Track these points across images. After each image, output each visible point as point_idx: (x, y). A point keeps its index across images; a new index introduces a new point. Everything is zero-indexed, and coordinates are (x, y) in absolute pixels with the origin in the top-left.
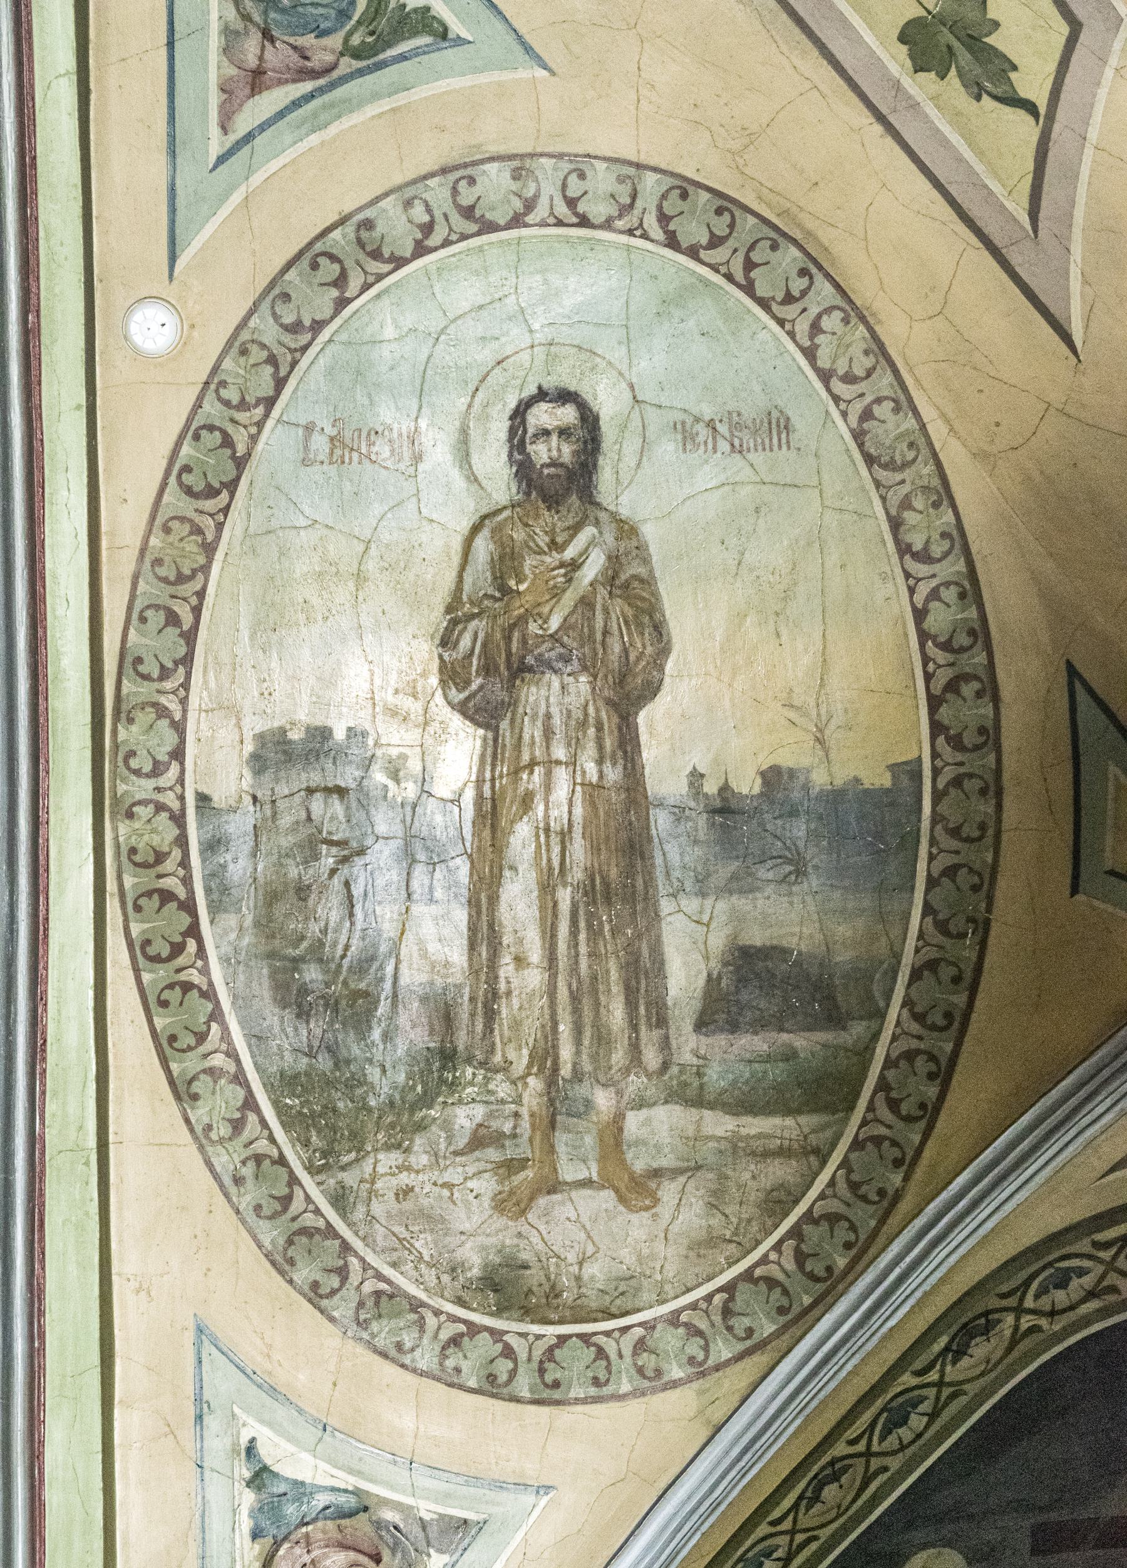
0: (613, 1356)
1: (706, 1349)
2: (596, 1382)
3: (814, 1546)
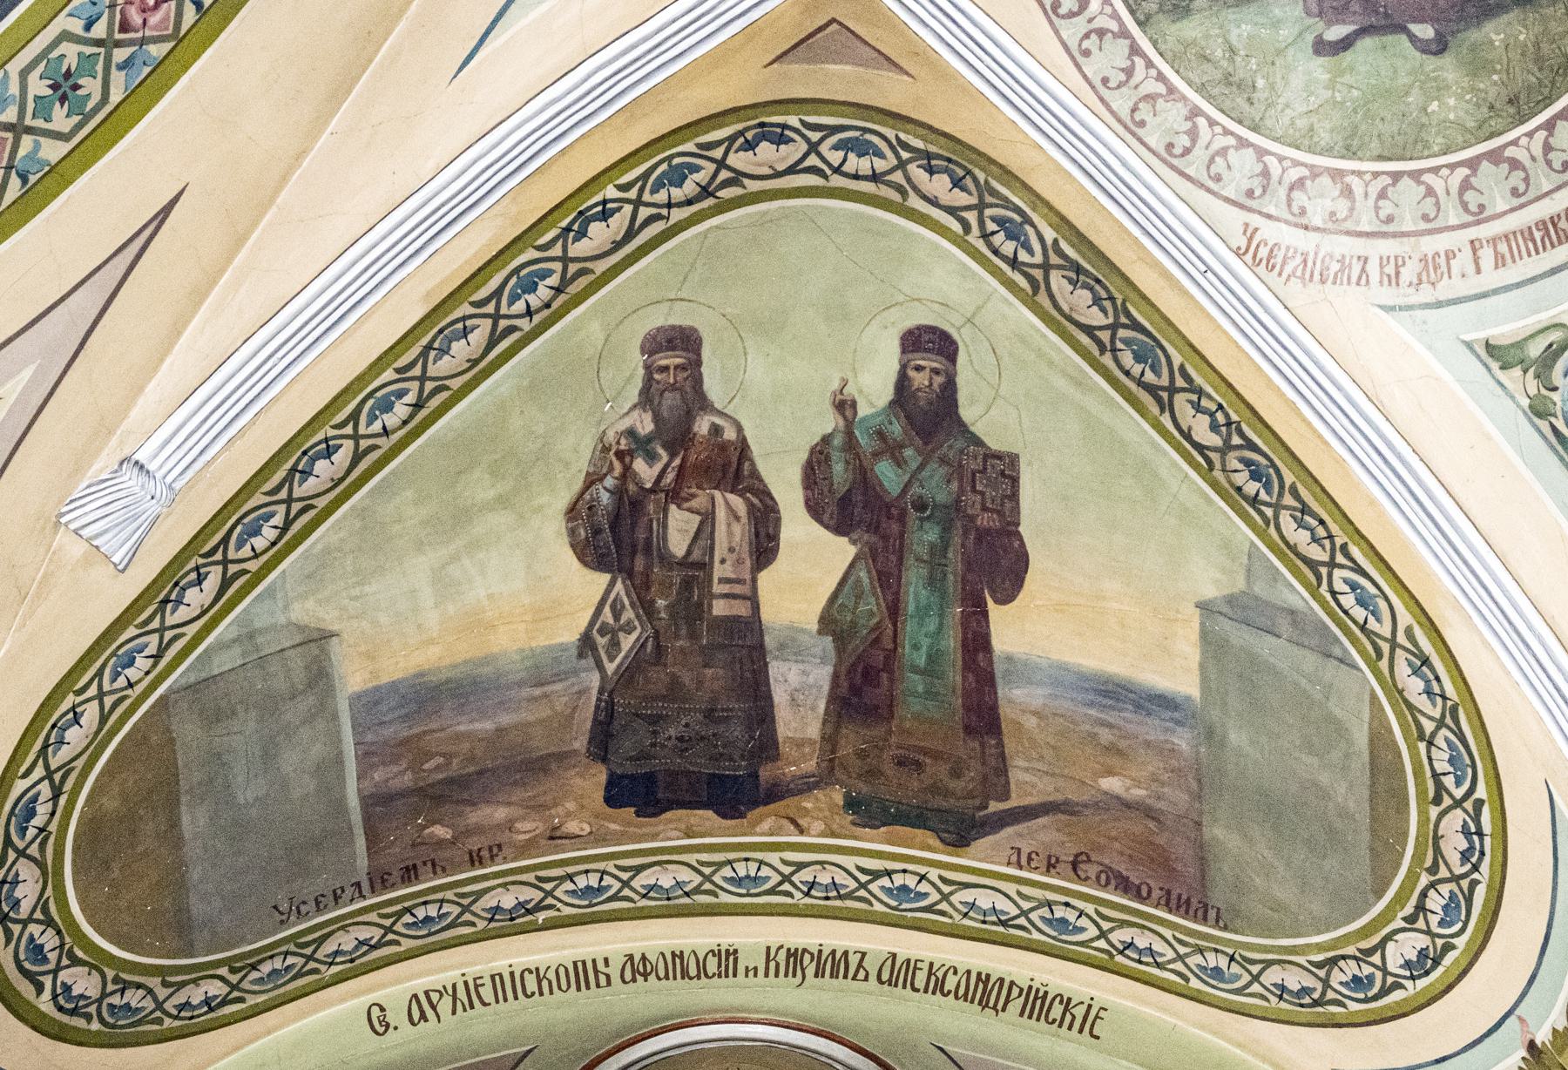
0: (1440, 192)
1: (1526, 180)
2: (1426, 218)
3: (268, 486)
